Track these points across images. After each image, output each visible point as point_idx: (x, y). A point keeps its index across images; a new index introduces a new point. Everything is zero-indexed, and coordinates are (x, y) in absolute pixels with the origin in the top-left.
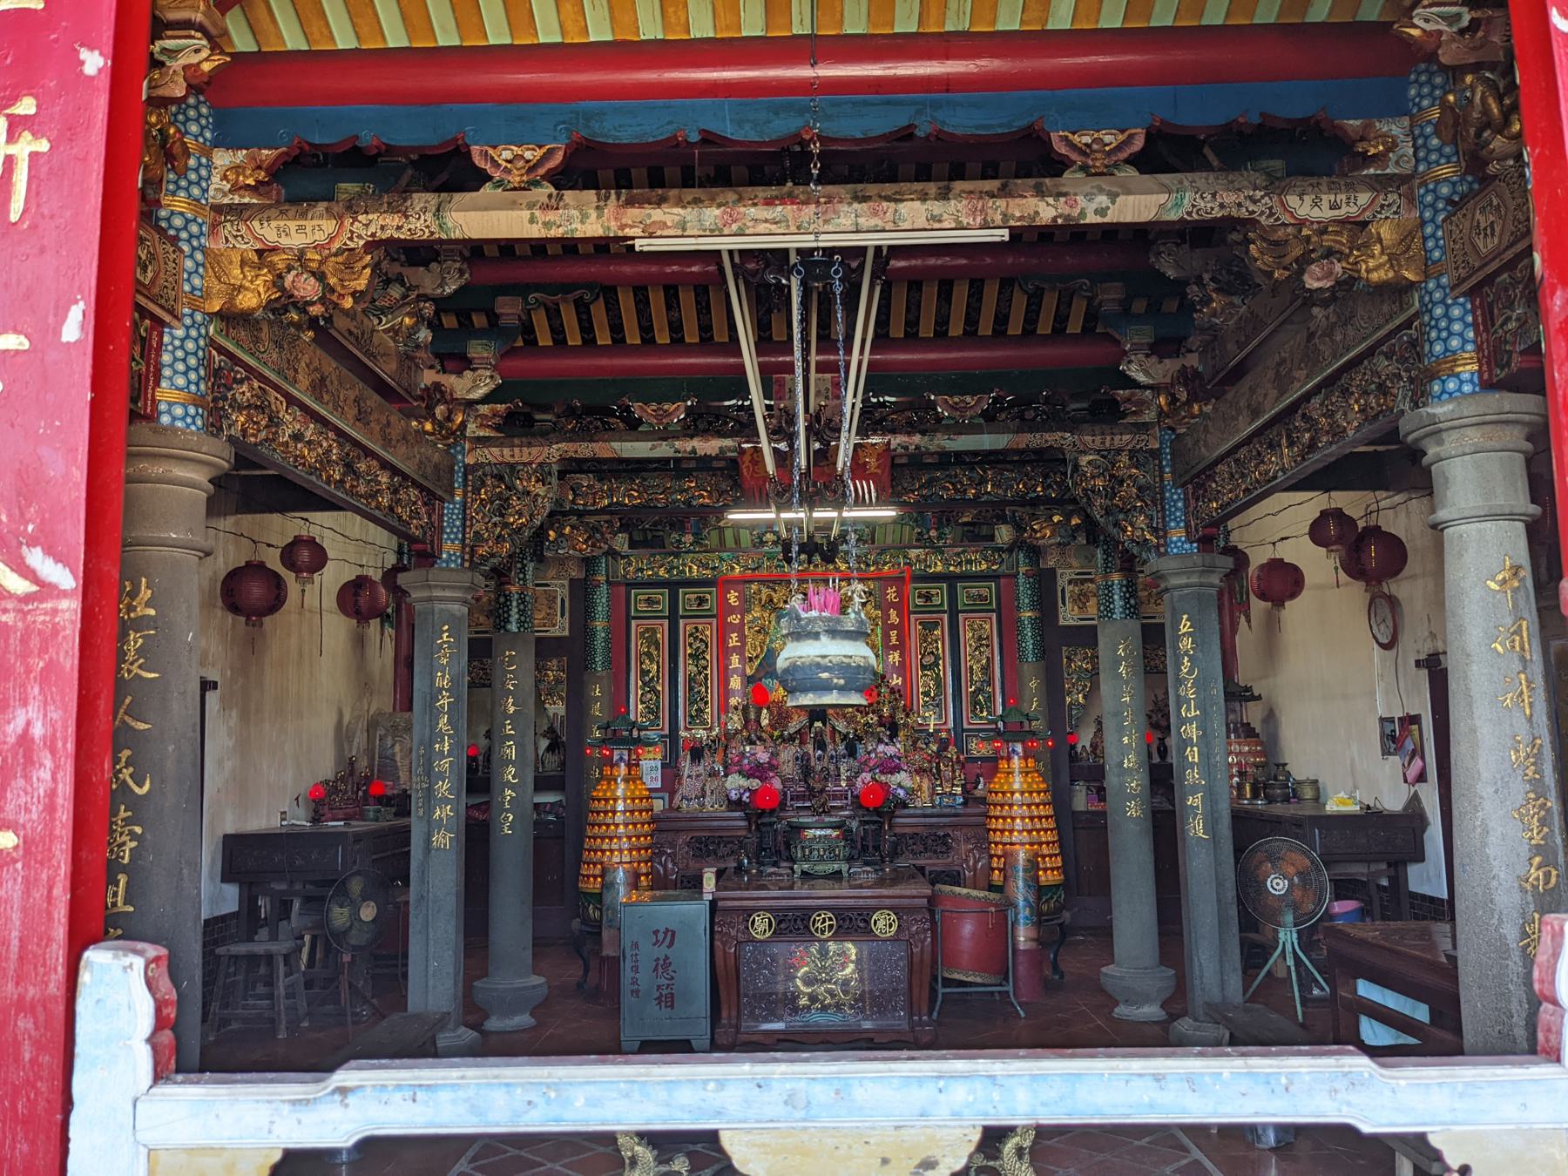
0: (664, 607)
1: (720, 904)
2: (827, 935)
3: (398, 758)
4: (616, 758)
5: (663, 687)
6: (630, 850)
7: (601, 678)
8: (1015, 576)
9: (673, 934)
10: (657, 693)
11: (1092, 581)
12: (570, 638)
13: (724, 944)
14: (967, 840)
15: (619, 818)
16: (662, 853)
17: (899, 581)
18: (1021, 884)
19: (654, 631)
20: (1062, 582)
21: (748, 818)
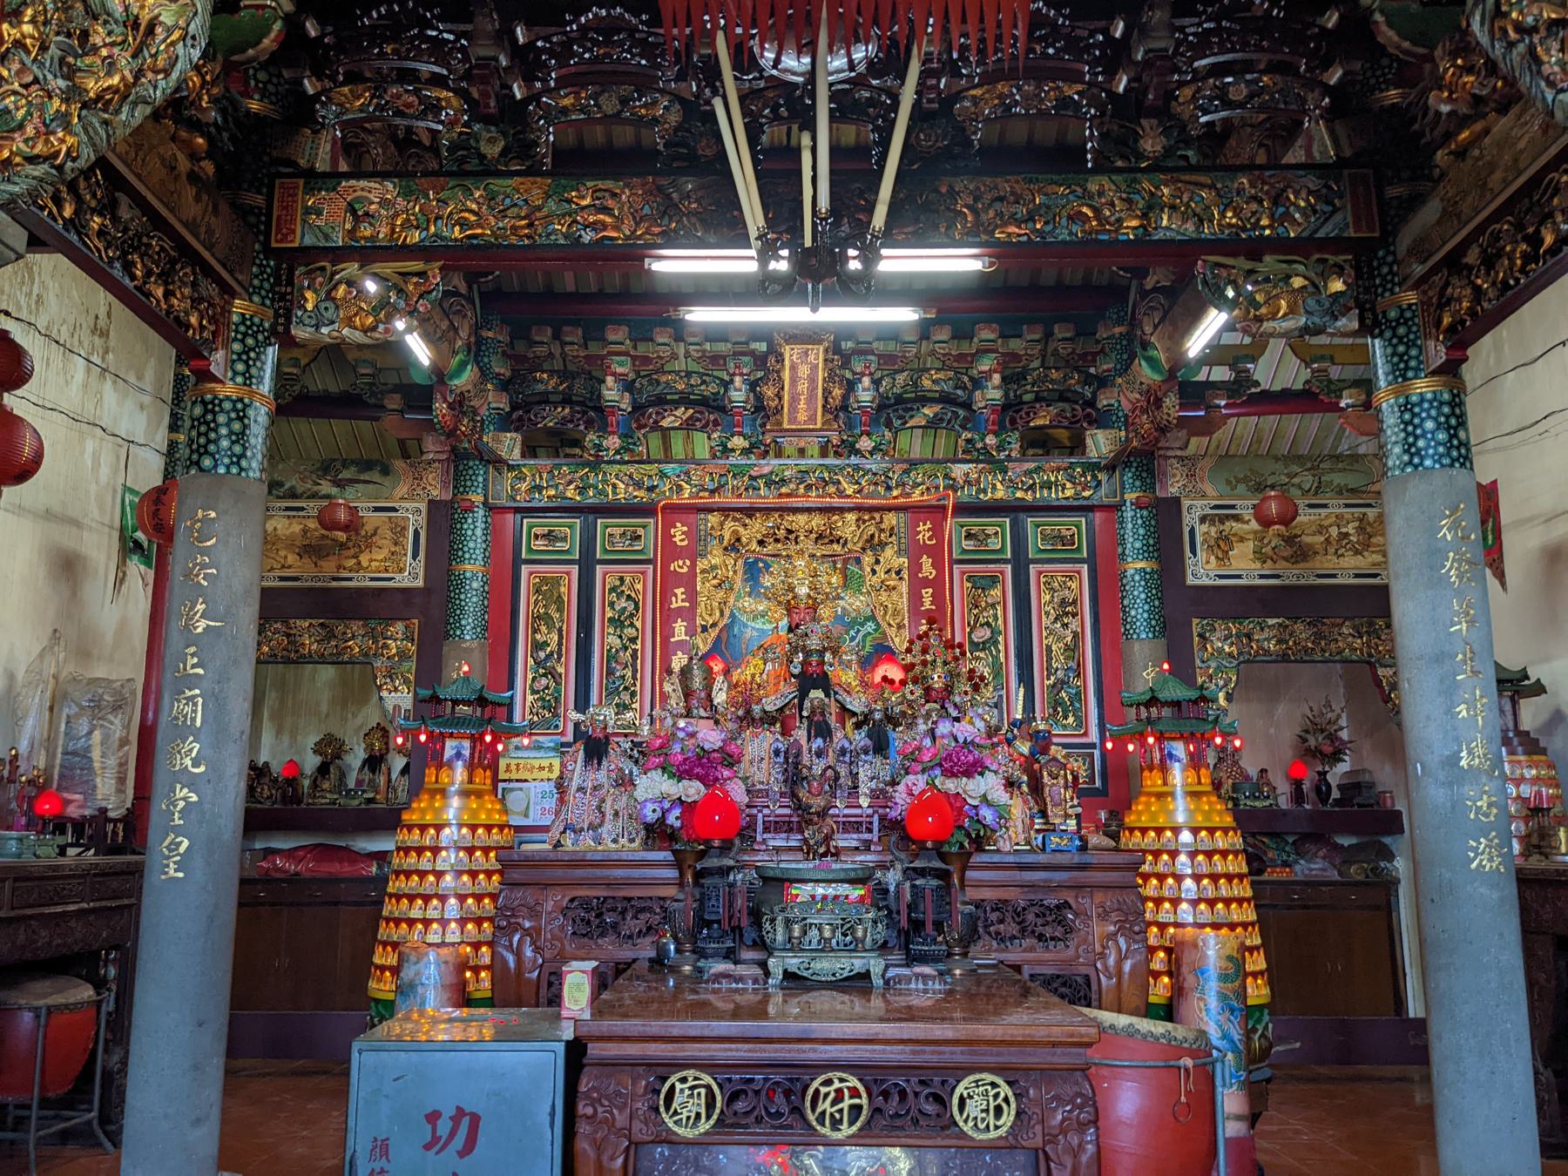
0: (572, 545)
1: (594, 1050)
2: (846, 1130)
3: (96, 754)
4: (449, 752)
5: (567, 668)
6: (462, 922)
7: (469, 650)
8: (1117, 508)
9: (475, 1120)
10: (556, 677)
11: (1237, 518)
12: (426, 591)
13: (599, 1148)
14: (1104, 916)
15: (448, 859)
16: (513, 928)
17: (935, 512)
18: (1213, 1002)
19: (556, 582)
20: (1190, 519)
21: (679, 864)
